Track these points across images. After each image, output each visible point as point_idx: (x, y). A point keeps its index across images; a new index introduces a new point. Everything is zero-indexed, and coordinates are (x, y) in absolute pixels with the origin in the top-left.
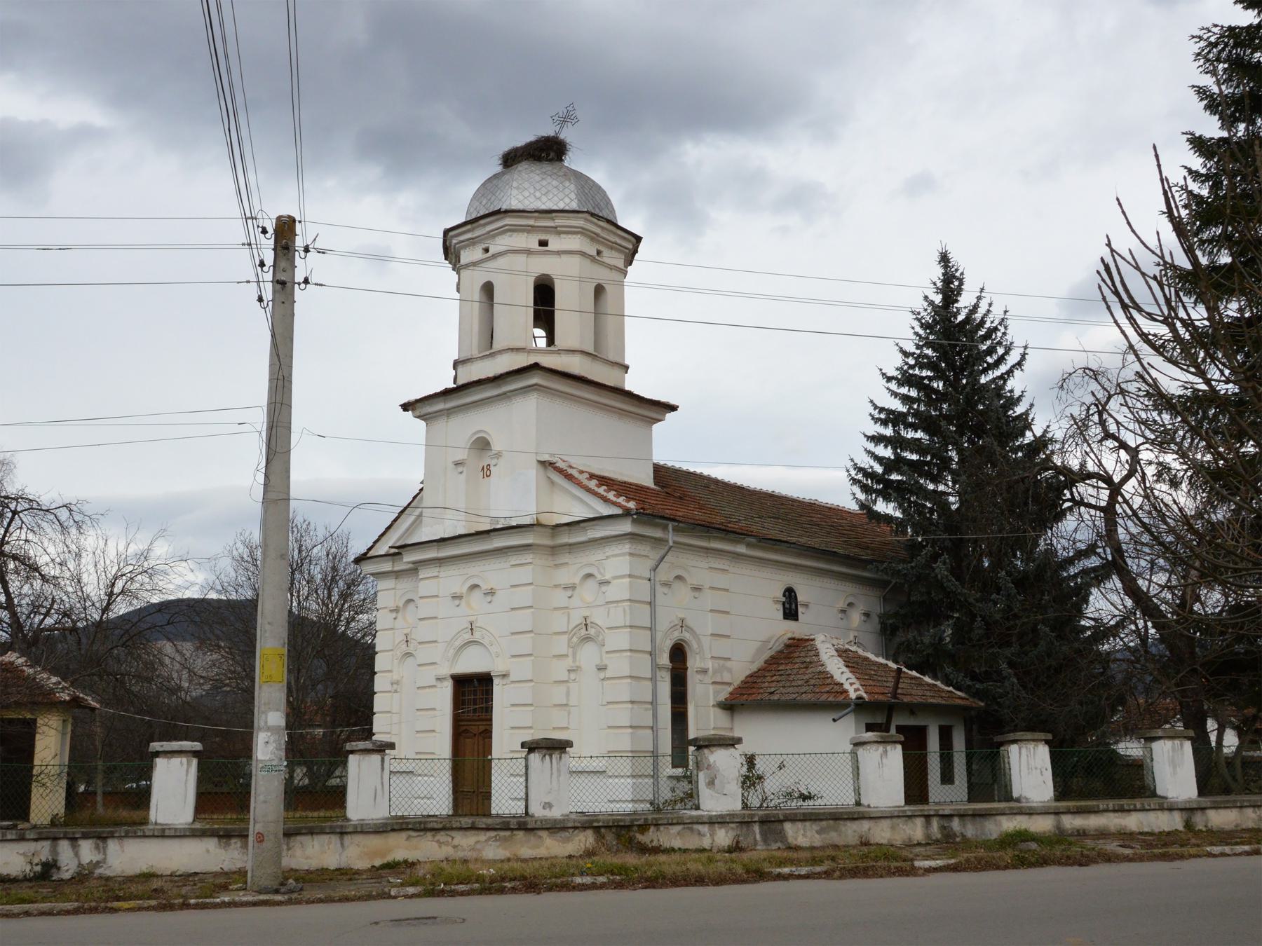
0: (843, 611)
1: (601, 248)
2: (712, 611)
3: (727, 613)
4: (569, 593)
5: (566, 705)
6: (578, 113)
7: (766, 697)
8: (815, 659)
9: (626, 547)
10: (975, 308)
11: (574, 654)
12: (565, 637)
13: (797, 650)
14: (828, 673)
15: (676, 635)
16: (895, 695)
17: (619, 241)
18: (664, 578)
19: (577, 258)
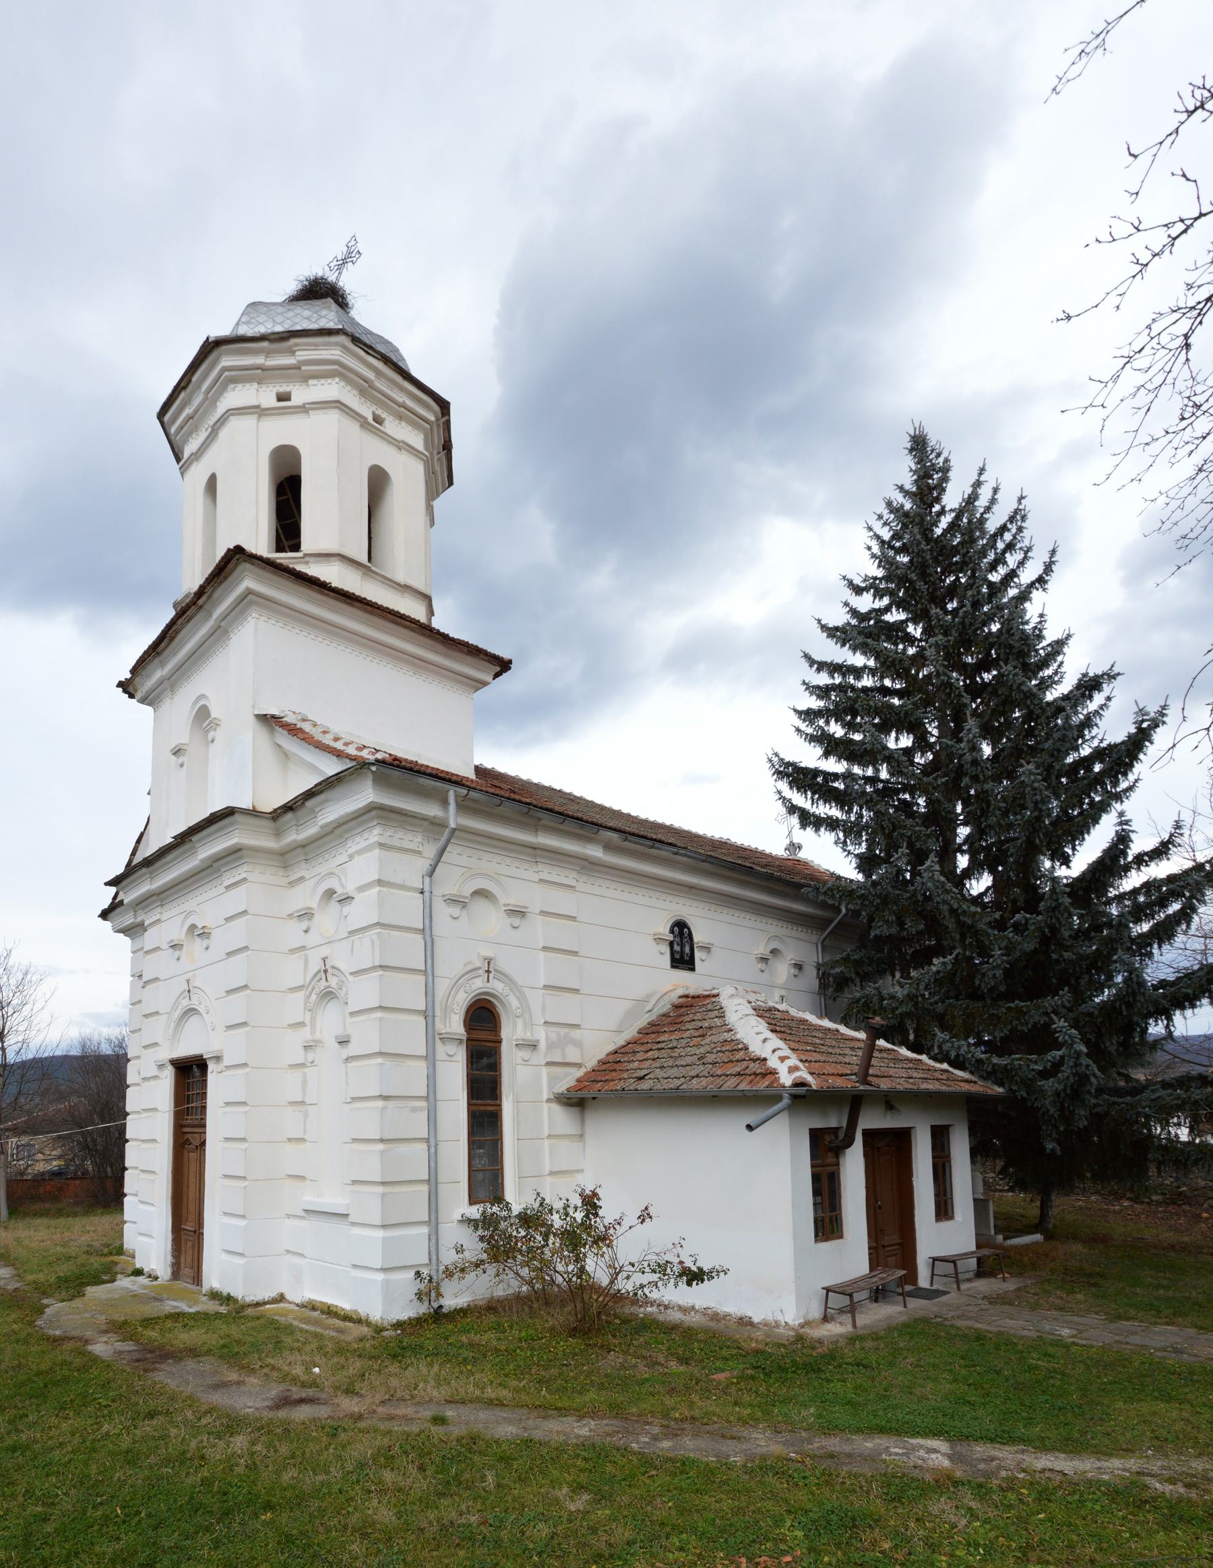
0: (764, 960)
1: (383, 414)
2: (545, 948)
3: (575, 953)
4: (305, 924)
5: (302, 1103)
6: (360, 247)
7: (631, 1084)
8: (718, 1022)
9: (375, 834)
10: (971, 500)
11: (313, 1020)
12: (301, 995)
13: (692, 1011)
14: (738, 1042)
15: (478, 985)
16: (864, 1077)
17: (410, 403)
18: (451, 889)
19: (334, 416)
